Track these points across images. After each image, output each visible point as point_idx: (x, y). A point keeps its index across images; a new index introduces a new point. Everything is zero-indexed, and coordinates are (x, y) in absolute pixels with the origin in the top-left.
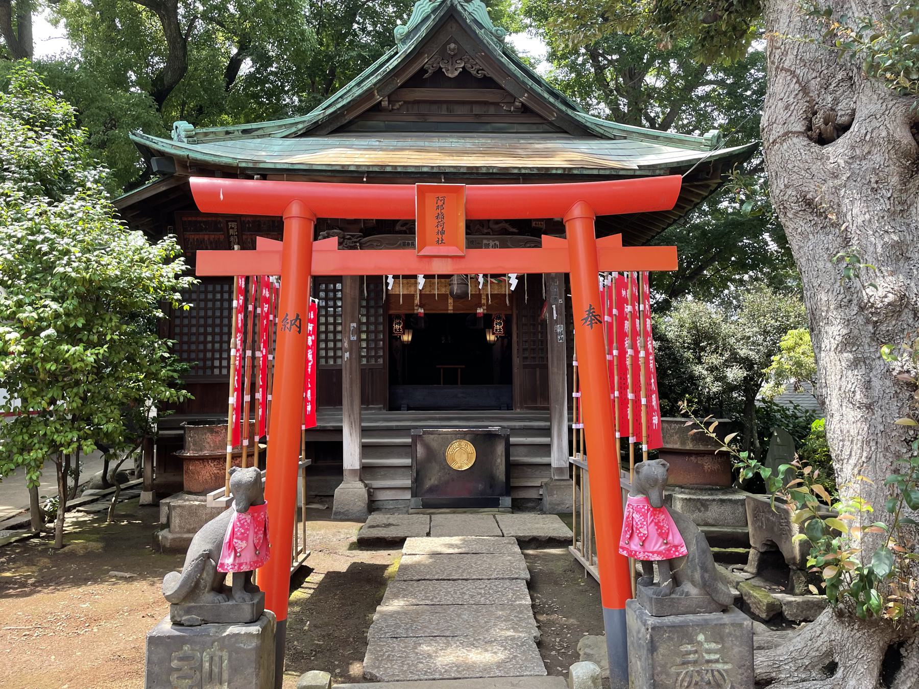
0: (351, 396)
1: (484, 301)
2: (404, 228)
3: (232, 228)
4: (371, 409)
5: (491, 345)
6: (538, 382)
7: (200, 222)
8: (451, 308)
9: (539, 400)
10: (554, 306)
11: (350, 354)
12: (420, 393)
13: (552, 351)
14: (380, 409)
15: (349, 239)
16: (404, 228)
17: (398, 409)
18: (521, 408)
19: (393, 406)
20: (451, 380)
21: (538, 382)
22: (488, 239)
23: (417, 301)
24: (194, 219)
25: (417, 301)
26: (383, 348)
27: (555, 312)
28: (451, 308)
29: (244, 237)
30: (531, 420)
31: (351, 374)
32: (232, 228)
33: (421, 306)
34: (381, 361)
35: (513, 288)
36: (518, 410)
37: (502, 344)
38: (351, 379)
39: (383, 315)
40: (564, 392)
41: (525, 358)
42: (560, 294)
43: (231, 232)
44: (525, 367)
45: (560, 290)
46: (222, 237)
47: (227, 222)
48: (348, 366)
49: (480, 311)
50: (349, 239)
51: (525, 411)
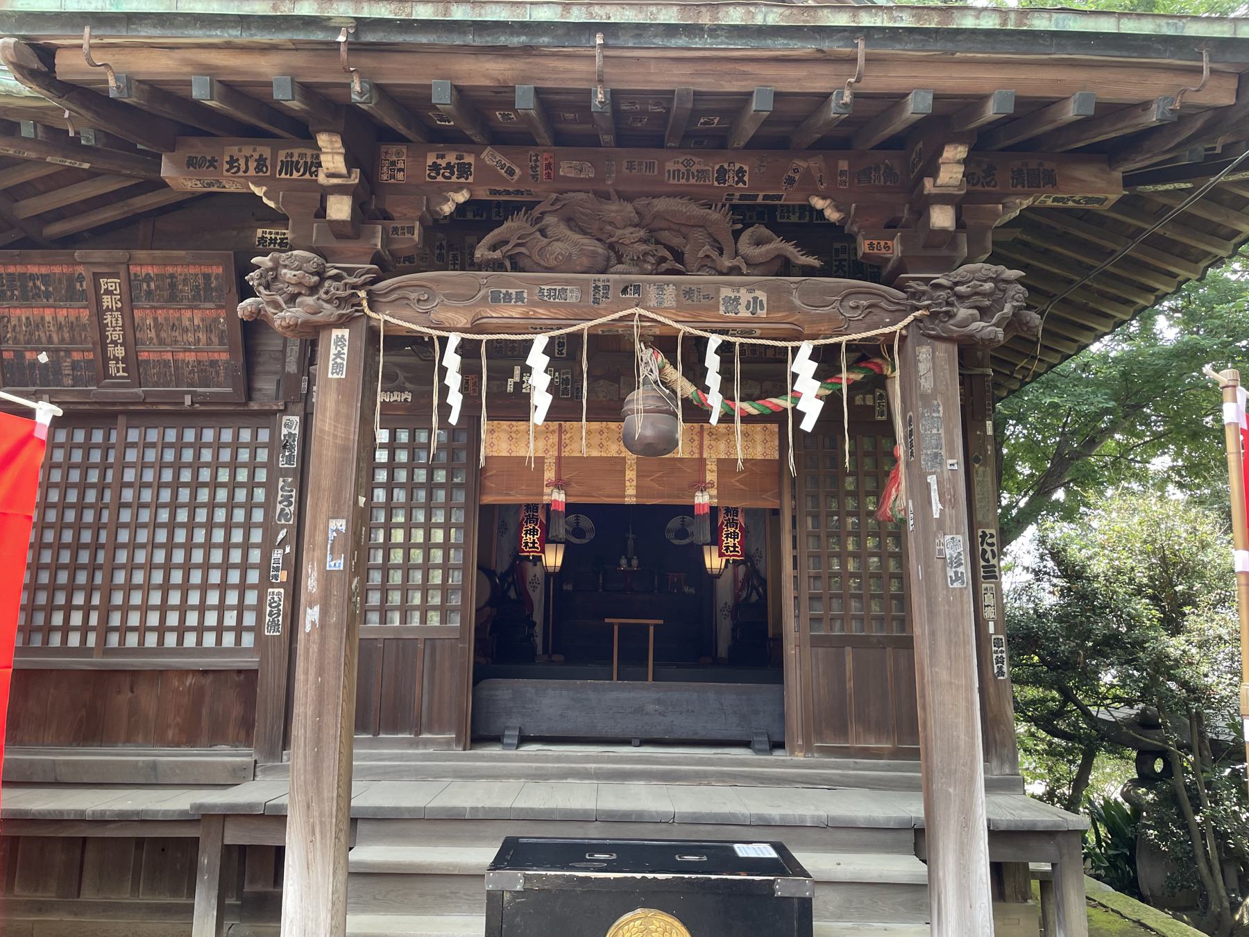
0: (318, 741)
1: (711, 477)
2: (497, 254)
3: (108, 292)
4: (426, 743)
5: (713, 577)
6: (850, 685)
7: (33, 277)
8: (631, 491)
9: (853, 729)
10: (932, 479)
11: (324, 613)
12: (550, 698)
13: (932, 614)
14: (448, 743)
15: (337, 278)
16: (497, 254)
17: (496, 739)
18: (808, 748)
19: (480, 734)
20: (632, 664)
21: (850, 685)
22: (736, 286)
23: (549, 475)
24: (20, 269)
25: (549, 475)
26: (463, 588)
27: (935, 496)
28: (631, 491)
29: (137, 313)
30: (823, 766)
31: (321, 671)
32: (108, 292)
33: (559, 484)
34: (456, 621)
35: (808, 425)
36: (800, 757)
37: (735, 575)
38: (320, 689)
39: (466, 507)
40: (972, 746)
41: (816, 620)
42: (951, 443)
43: (107, 301)
44: (816, 642)
45: (949, 432)
46: (85, 314)
47: (97, 277)
48: (314, 648)
49: (702, 499)
50: (337, 278)
51: (817, 758)
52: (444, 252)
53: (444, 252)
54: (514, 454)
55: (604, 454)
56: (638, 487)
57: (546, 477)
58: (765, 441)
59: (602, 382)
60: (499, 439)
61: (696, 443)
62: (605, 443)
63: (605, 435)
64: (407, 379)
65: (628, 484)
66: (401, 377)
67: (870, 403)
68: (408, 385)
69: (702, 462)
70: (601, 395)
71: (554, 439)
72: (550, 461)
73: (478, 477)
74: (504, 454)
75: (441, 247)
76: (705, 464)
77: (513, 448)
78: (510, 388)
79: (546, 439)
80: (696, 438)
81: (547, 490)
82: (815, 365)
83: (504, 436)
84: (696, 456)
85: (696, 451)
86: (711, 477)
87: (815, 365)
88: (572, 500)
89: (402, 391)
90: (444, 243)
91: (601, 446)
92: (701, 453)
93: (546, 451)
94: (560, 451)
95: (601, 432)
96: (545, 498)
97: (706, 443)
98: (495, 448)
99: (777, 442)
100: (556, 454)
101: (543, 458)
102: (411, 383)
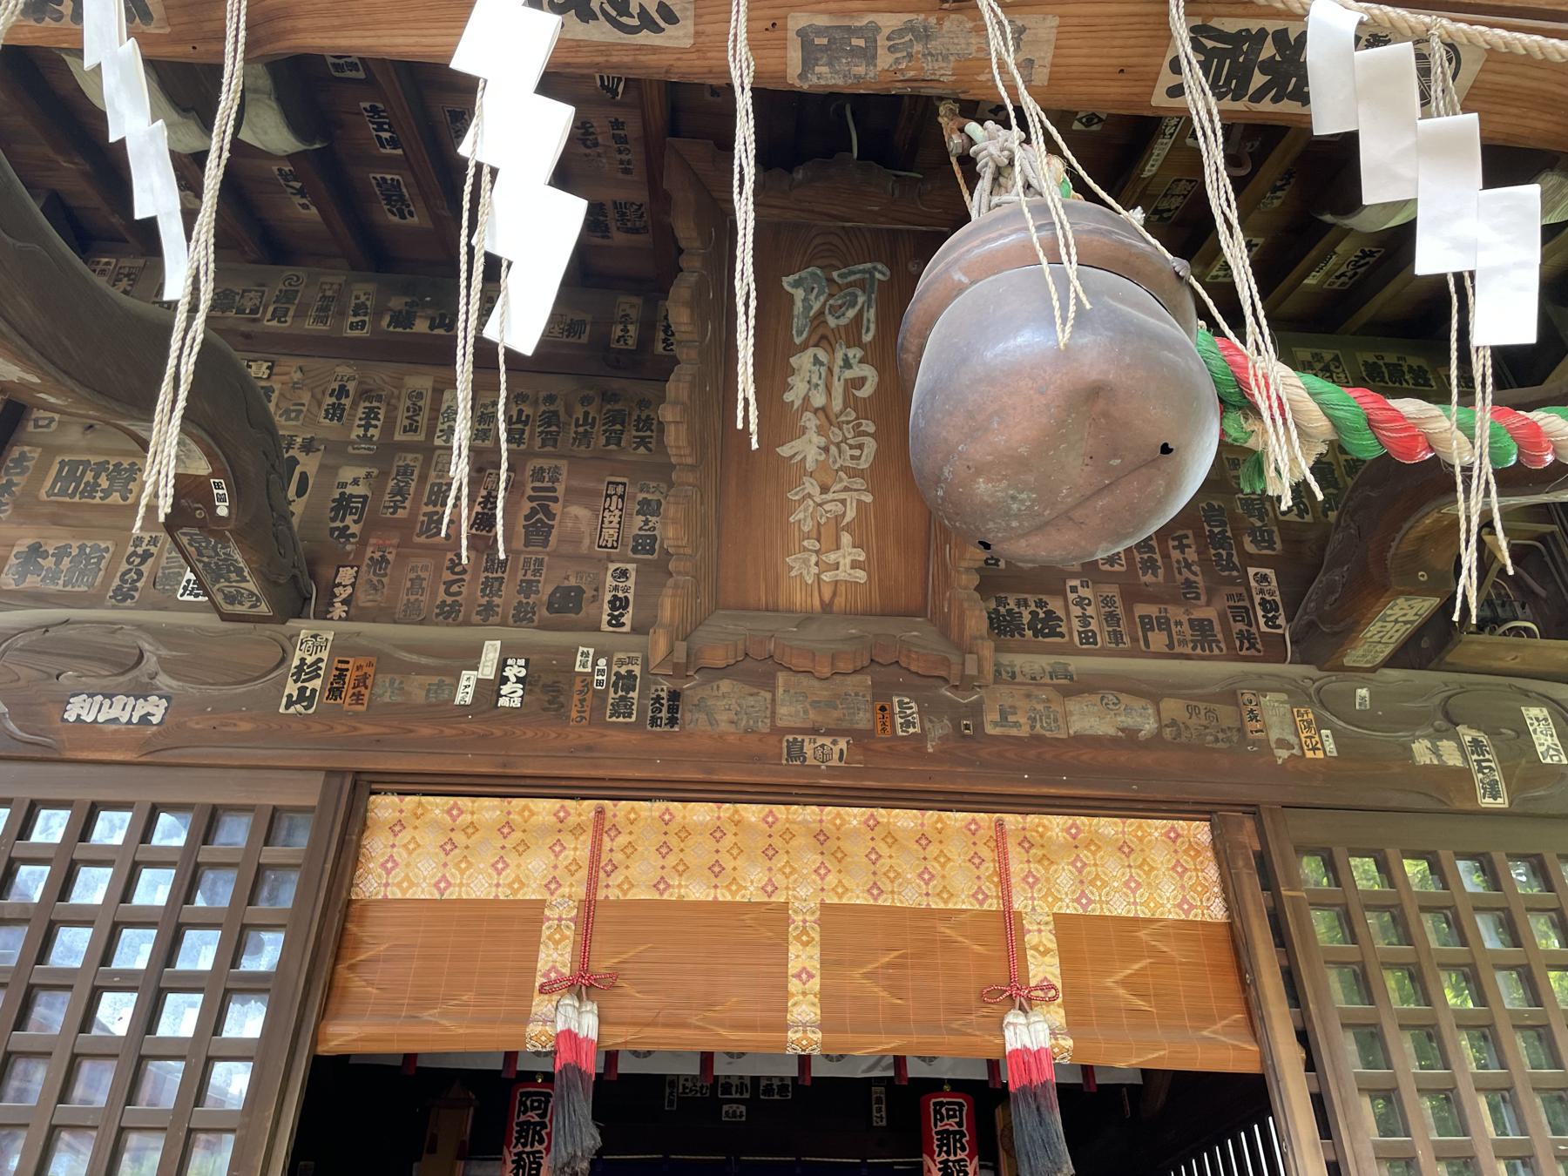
1: (1043, 968)
25: (555, 957)
26: (241, 1124)
33: (582, 984)
52: (346, 402)
53: (346, 402)
54: (452, 894)
55: (724, 896)
56: (825, 997)
57: (542, 965)
58: (1179, 869)
59: (725, 685)
60: (414, 847)
61: (989, 867)
62: (729, 864)
63: (729, 840)
64: (167, 666)
65: (794, 985)
66: (150, 663)
67: (1454, 759)
68: (163, 680)
69: (1009, 923)
70: (723, 717)
71: (578, 849)
72: (562, 910)
73: (332, 930)
74: (424, 892)
75: (342, 392)
76: (1023, 932)
77: (453, 874)
78: (464, 693)
79: (557, 848)
80: (985, 852)
81: (541, 1005)
82: (139, 215)
83: (430, 840)
84: (993, 905)
85: (991, 889)
86: (1043, 968)
87: (139, 215)
88: (620, 1037)
89: (141, 693)
90: (351, 386)
91: (716, 869)
92: (1006, 897)
93: (553, 884)
94: (592, 883)
95: (717, 833)
96: (533, 1029)
97: (1016, 867)
98: (398, 874)
99: (1212, 872)
100: (581, 892)
101: (542, 904)
102: (173, 674)
